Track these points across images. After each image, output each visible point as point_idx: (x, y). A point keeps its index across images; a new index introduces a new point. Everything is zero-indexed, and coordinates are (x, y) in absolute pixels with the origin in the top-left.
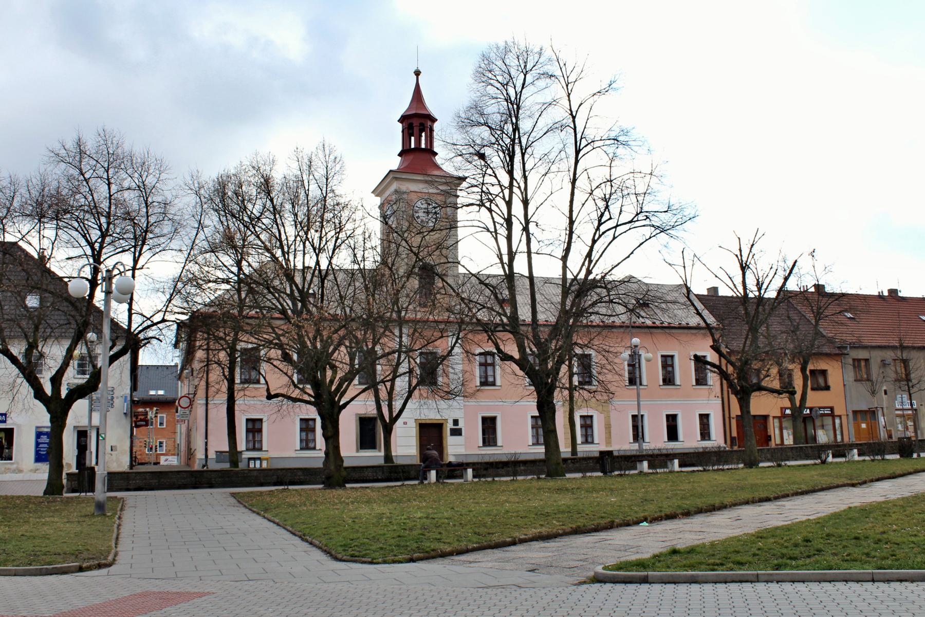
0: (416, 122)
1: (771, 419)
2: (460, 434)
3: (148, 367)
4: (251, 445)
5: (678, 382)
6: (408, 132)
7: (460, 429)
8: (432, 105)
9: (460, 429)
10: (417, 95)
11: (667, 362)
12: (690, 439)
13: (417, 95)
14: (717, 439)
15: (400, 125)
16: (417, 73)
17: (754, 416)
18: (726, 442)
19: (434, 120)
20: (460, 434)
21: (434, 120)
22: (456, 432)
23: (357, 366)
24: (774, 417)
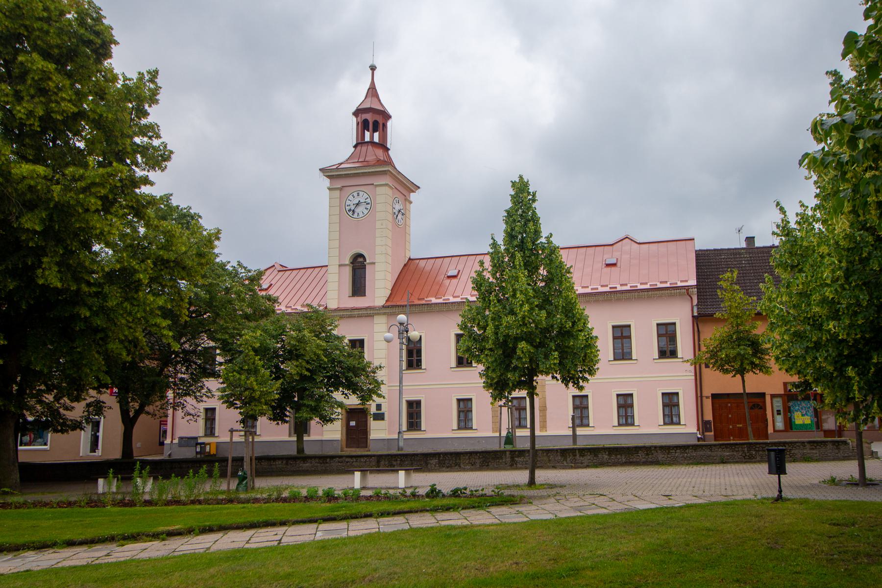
0: (369, 117)
1: (768, 398)
2: (383, 419)
3: (548, 451)
4: (517, 423)
5: (634, 357)
6: (364, 126)
7: (383, 414)
8: (388, 101)
9: (383, 414)
10: (372, 91)
11: (622, 334)
12: (649, 423)
13: (372, 91)
14: (688, 426)
15: (355, 119)
16: (373, 68)
17: (123, 456)
18: (698, 430)
19: (389, 117)
20: (383, 419)
21: (389, 117)
22: (379, 417)
23: (96, 248)
24: (773, 396)
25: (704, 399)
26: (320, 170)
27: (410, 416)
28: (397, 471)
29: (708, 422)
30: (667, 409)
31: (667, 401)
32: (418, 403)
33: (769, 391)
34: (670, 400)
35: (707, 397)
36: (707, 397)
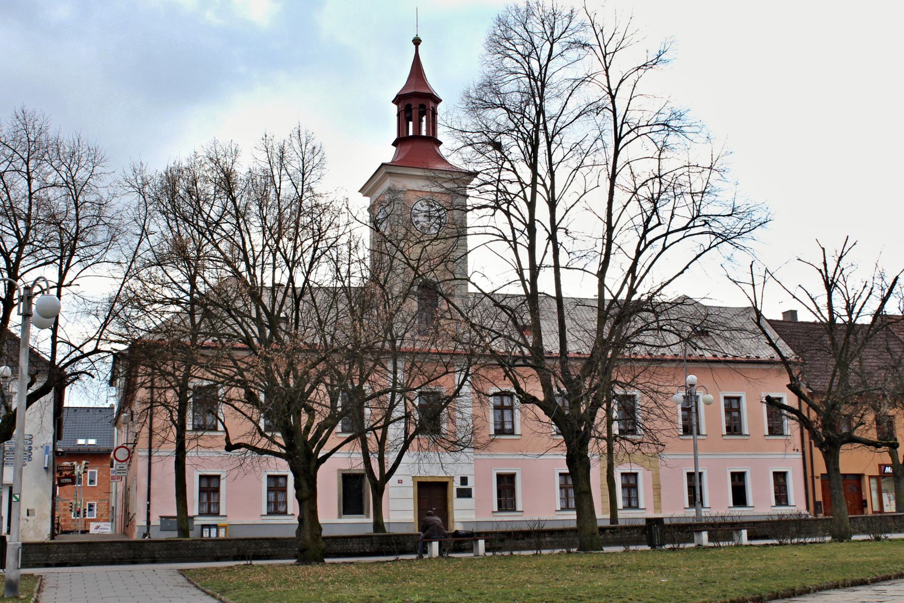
1: (866, 479)
2: (470, 496)
6: (405, 116)
7: (470, 490)
9: (470, 490)
12: (761, 504)
14: (797, 504)
15: (395, 107)
18: (808, 508)
19: (437, 101)
20: (470, 496)
21: (437, 101)
24: (870, 477)
25: (815, 479)
26: (360, 191)
27: (692, 489)
28: (701, 531)
29: (820, 502)
30: (272, 495)
31: (205, 484)
32: (511, 477)
33: (868, 473)
34: (277, 483)
35: (817, 478)
36: (817, 478)
